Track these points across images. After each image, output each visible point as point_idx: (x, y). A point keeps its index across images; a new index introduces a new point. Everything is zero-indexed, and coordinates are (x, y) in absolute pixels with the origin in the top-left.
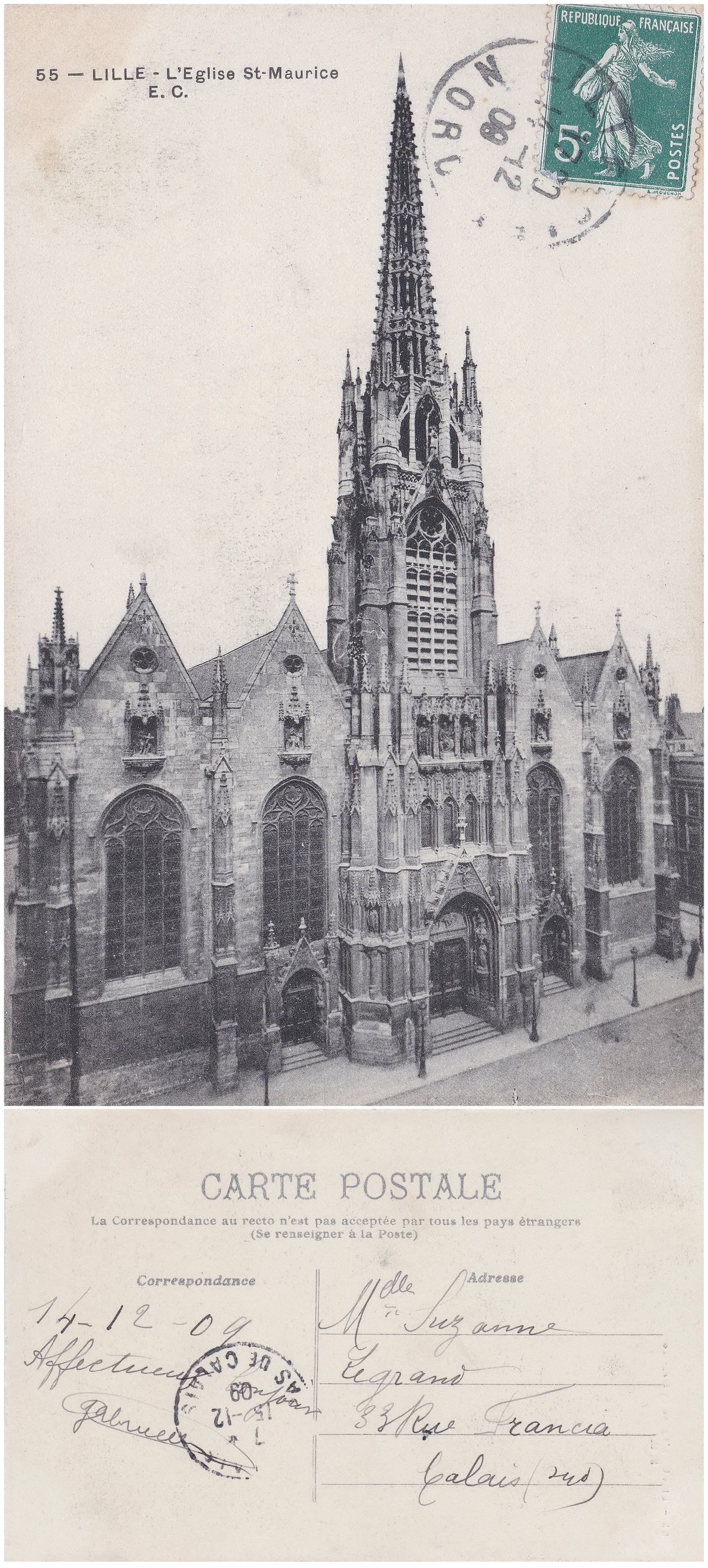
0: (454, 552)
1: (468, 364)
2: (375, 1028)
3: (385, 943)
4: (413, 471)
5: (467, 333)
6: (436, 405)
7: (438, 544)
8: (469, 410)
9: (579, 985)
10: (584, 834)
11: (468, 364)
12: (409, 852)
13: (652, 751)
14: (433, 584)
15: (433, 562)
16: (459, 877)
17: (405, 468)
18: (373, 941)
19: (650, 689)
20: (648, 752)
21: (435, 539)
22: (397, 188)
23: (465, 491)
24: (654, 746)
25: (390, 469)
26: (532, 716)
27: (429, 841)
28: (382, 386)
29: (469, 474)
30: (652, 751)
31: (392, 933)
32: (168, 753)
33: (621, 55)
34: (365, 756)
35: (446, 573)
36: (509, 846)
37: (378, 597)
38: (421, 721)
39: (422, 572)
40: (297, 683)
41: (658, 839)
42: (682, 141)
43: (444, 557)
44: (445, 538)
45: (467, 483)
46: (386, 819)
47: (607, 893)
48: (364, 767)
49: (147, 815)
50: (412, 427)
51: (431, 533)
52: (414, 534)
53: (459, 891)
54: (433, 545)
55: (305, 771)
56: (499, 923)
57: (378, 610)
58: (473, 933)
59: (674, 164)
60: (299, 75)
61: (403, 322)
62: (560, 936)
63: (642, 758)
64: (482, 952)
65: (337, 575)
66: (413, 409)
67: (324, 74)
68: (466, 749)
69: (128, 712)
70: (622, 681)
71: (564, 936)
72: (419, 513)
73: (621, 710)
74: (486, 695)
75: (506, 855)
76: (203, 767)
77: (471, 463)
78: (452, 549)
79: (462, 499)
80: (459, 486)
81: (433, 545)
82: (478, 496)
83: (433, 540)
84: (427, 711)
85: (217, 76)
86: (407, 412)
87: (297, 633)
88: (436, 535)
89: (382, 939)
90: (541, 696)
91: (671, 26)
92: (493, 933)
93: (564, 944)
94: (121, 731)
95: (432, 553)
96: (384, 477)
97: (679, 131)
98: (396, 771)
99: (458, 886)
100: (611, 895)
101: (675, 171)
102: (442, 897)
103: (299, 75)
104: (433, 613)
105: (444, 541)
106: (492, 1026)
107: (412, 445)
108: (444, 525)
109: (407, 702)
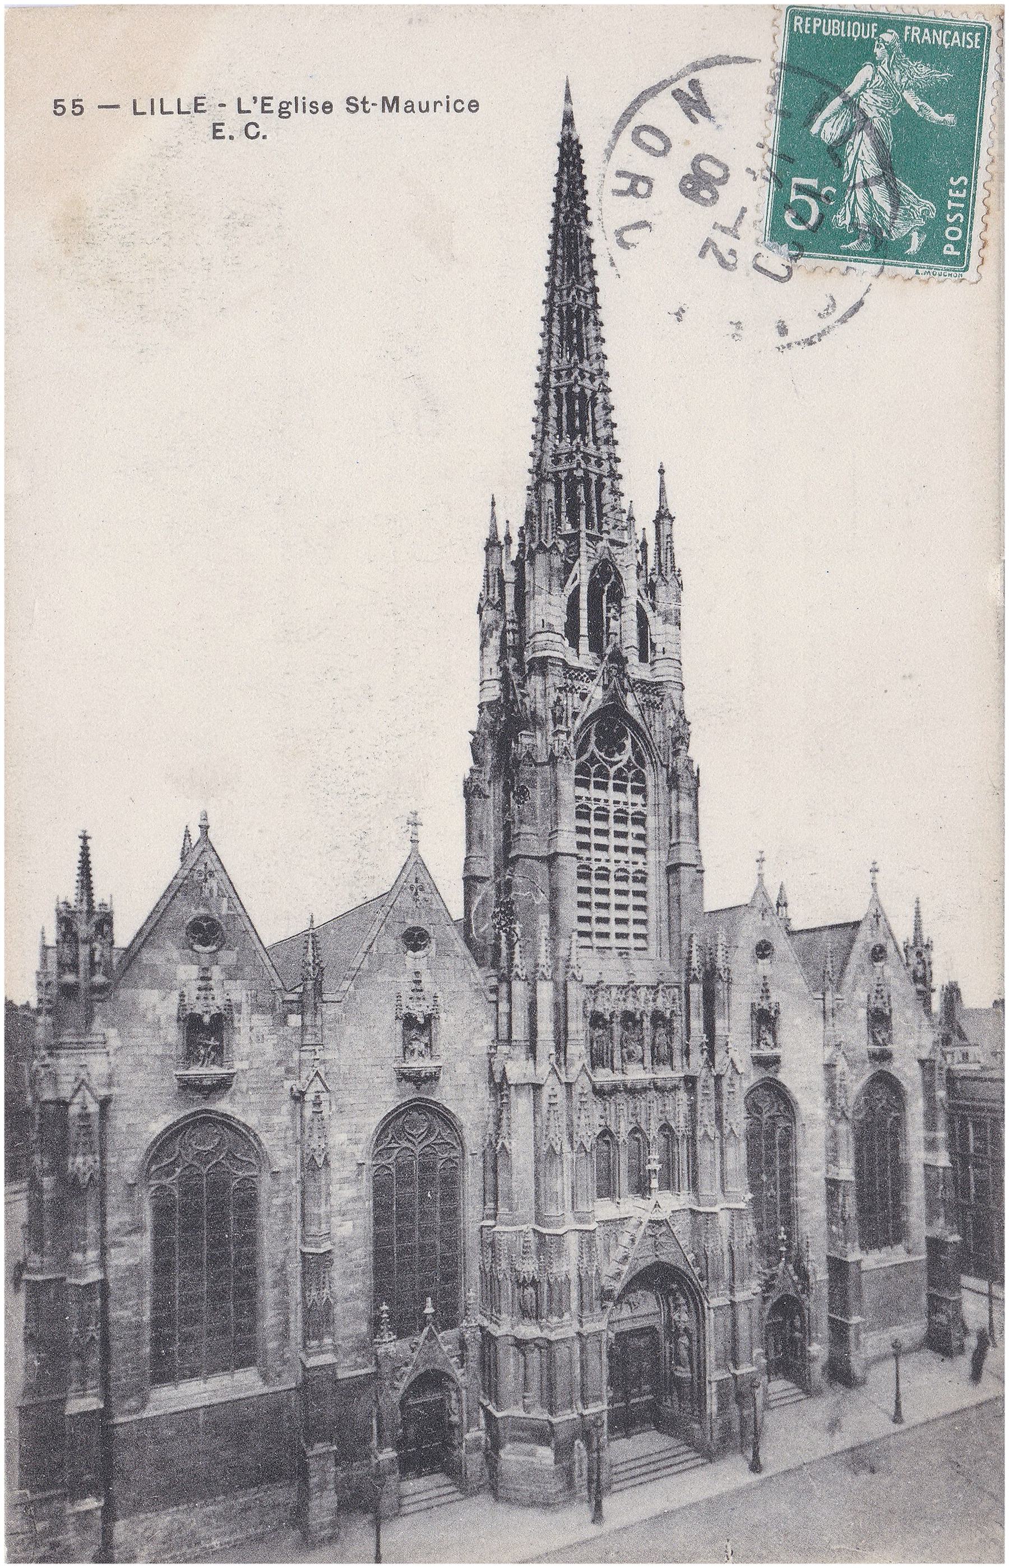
0: (643, 781)
1: (663, 516)
2: (532, 1454)
3: (545, 1334)
5: (662, 472)
6: (618, 574)
7: (620, 770)
8: (664, 580)
9: (819, 1392)
10: (826, 1179)
11: (663, 516)
14: (613, 826)
15: (613, 795)
18: (529, 1331)
19: (919, 975)
20: (916, 1064)
21: (617, 763)
22: (563, 267)
24: (924, 1055)
25: (552, 665)
26: (753, 1013)
27: (607, 1189)
28: (541, 546)
29: (664, 671)
31: (556, 1319)
32: (238, 1066)
33: (878, 79)
34: (518, 1070)
35: (631, 810)
36: (720, 1196)
37: (536, 844)
38: (596, 1020)
39: (598, 809)
40: (422, 966)
41: (931, 1186)
42: (965, 201)
43: (629, 788)
44: (629, 761)
45: (661, 683)
47: (858, 1263)
48: (516, 1086)
49: (209, 1152)
50: (584, 604)
51: (611, 754)
52: (586, 756)
53: (650, 1261)
54: (612, 771)
55: (431, 1091)
56: (706, 1305)
57: (536, 863)
58: (670, 1319)
59: (953, 234)
60: (424, 108)
62: (792, 1324)
64: (682, 1347)
66: (585, 579)
67: (459, 106)
69: (182, 1007)
70: (880, 964)
71: (798, 1324)
73: (879, 1004)
74: (688, 983)
76: (288, 1084)
78: (640, 777)
79: (653, 706)
81: (612, 771)
83: (613, 764)
84: (605, 1006)
85: (308, 108)
86: (576, 583)
87: (420, 894)
88: (617, 757)
89: (541, 1328)
90: (765, 985)
91: (949, 38)
92: (698, 1320)
94: (173, 1034)
96: (544, 675)
97: (960, 187)
98: (561, 1091)
99: (648, 1253)
100: (864, 1266)
101: (954, 243)
102: (626, 1268)
103: (424, 108)
104: (612, 867)
106: (697, 1451)
107: (584, 630)
108: (628, 743)
109: (576, 993)
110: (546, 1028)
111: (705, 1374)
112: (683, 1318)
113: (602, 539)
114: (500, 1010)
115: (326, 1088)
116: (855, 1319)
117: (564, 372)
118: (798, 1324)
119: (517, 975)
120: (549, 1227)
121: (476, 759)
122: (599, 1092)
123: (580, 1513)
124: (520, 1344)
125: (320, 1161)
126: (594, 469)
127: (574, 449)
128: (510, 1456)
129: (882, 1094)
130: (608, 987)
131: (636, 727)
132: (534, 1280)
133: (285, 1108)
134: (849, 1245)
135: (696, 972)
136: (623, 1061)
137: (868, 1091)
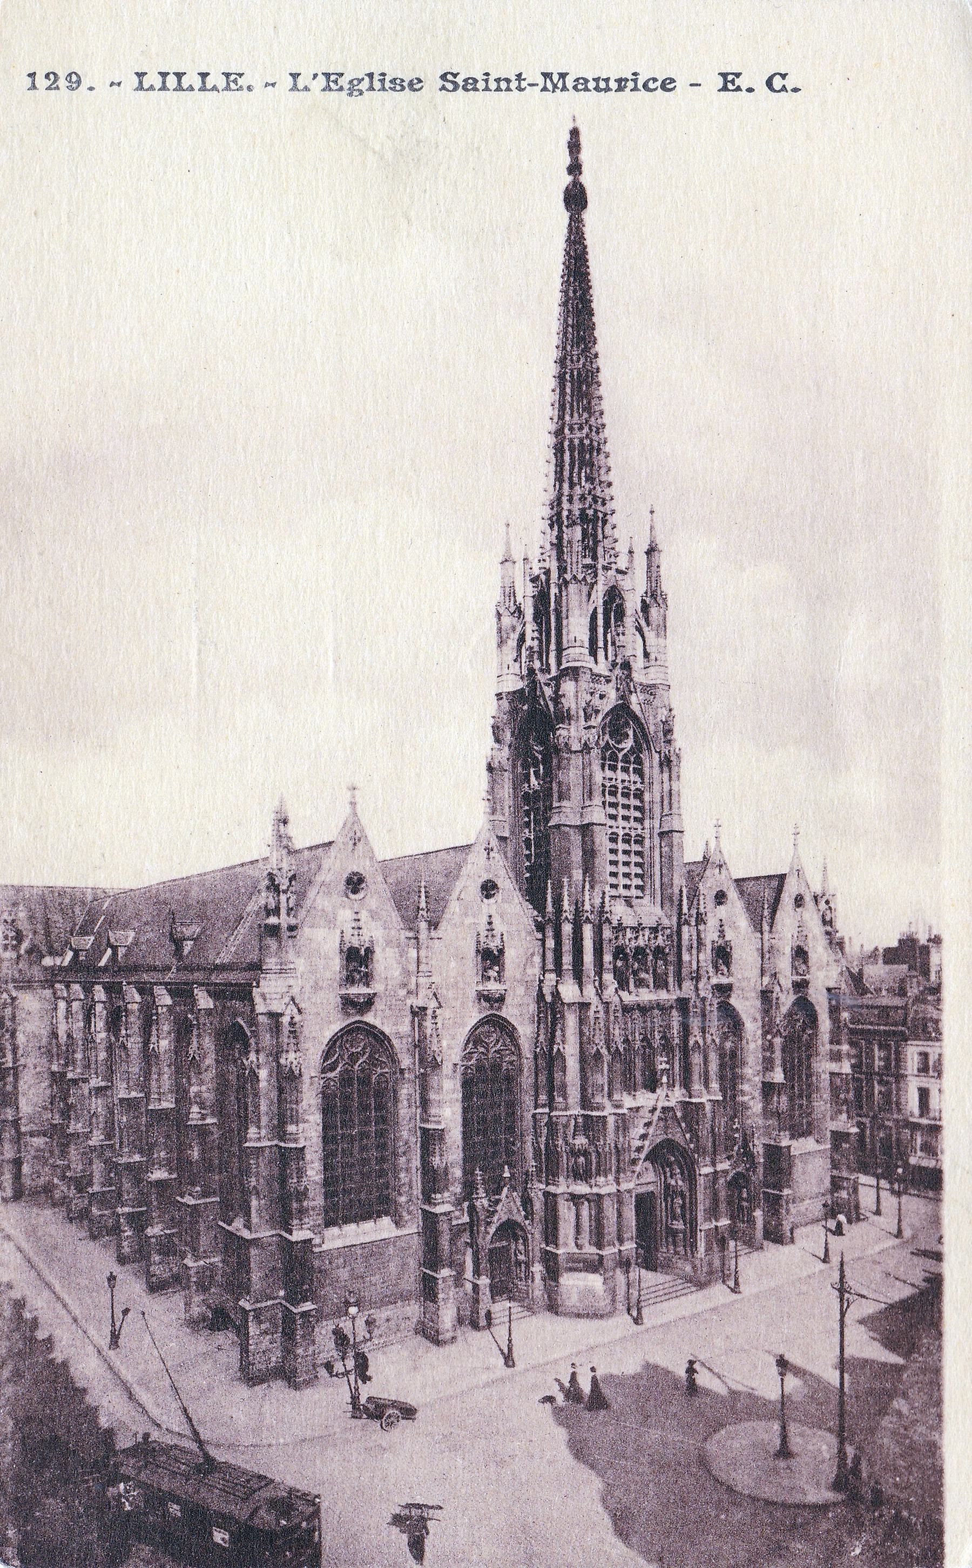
3: (595, 1190)
4: (602, 673)
6: (622, 598)
10: (762, 1082)
13: (829, 990)
14: (621, 800)
15: (621, 775)
16: (662, 1124)
17: (596, 671)
18: (581, 1188)
19: (828, 919)
21: (623, 749)
23: (651, 694)
24: (832, 984)
26: (478, 951)
28: (575, 577)
29: (653, 677)
30: (829, 990)
34: (569, 991)
36: (704, 1092)
38: (619, 952)
39: (611, 786)
41: (835, 1090)
43: (631, 769)
46: (588, 1061)
51: (619, 742)
54: (620, 756)
55: (500, 1008)
63: (819, 999)
68: (660, 983)
74: (679, 926)
75: (703, 1100)
76: (409, 1002)
77: (658, 663)
78: (639, 761)
79: (649, 703)
80: (650, 689)
81: (620, 756)
84: (630, 941)
87: (491, 853)
89: (591, 1187)
90: (721, 926)
93: (745, 1204)
94: (337, 963)
95: (620, 765)
99: (658, 1132)
104: (621, 832)
105: (632, 751)
108: (631, 733)
109: (607, 933)
110: (567, 959)
114: (547, 946)
117: (576, 426)
118: (745, 1195)
119: (566, 918)
121: (498, 740)
122: (626, 1009)
124: (575, 1199)
125: (297, 1072)
126: (600, 508)
131: (636, 718)
132: (585, 1150)
133: (408, 1020)
135: (567, 914)
137: (475, 1039)
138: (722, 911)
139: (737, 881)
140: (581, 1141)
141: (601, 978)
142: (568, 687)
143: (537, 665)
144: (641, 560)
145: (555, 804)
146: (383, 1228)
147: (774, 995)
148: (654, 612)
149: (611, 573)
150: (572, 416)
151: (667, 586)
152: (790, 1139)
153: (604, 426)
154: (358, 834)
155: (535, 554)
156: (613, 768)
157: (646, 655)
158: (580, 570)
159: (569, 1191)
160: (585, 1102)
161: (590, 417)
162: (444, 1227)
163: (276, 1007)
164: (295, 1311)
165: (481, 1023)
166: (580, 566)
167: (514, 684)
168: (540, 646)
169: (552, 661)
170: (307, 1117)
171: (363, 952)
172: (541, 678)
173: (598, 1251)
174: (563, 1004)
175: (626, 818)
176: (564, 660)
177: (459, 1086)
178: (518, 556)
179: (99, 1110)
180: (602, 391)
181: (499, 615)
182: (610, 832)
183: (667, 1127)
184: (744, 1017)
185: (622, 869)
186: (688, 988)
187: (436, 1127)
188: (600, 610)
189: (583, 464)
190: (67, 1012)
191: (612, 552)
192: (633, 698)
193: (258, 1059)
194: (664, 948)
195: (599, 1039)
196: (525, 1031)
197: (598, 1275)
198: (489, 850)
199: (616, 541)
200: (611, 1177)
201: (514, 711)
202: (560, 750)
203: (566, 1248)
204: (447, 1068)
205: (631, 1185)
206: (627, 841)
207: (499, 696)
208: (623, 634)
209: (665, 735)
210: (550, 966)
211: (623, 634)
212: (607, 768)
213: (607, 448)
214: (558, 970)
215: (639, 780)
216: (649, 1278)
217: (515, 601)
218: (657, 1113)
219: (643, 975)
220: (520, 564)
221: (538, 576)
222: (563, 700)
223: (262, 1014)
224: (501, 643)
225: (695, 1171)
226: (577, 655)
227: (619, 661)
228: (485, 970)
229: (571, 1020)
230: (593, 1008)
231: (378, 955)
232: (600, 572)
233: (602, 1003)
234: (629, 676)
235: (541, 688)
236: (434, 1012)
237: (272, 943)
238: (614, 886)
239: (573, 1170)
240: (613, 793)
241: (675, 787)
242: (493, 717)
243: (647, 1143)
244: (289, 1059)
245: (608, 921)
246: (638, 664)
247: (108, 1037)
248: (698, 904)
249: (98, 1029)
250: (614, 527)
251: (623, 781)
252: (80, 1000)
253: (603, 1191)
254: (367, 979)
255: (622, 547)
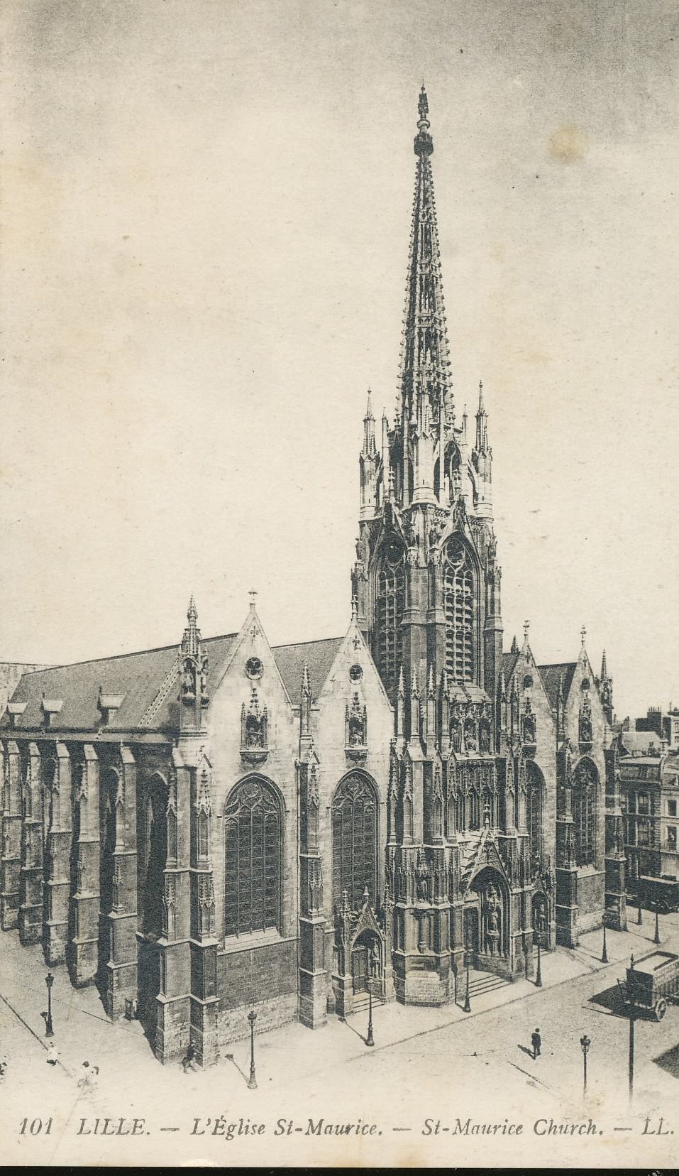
0: (471, 578)
6: (458, 451)
7: (459, 571)
9: (555, 950)
12: (450, 835)
15: (456, 587)
16: (485, 855)
18: (425, 905)
19: (606, 698)
21: (458, 566)
24: (608, 747)
29: (482, 511)
32: (270, 747)
34: (415, 752)
38: (454, 723)
43: (455, 580)
45: (481, 518)
47: (575, 872)
51: (455, 561)
54: (456, 571)
61: (429, 373)
64: (494, 918)
65: (360, 589)
68: (484, 747)
70: (587, 691)
71: (543, 910)
72: (447, 544)
80: (479, 520)
81: (456, 571)
82: (491, 530)
83: (456, 567)
88: (458, 564)
99: (483, 861)
105: (464, 568)
106: (502, 977)
111: (509, 933)
112: (496, 901)
113: (450, 428)
115: (318, 761)
116: (574, 906)
118: (543, 910)
120: (433, 845)
121: (359, 557)
123: (454, 1011)
124: (418, 914)
126: (442, 382)
127: (432, 369)
128: (412, 978)
129: (358, 791)
130: (459, 704)
134: (571, 862)
136: (466, 749)
138: (528, 693)
139: (540, 667)
140: (424, 868)
141: (440, 743)
142: (418, 518)
143: (393, 500)
144: (472, 422)
145: (407, 608)
146: (270, 936)
147: (567, 755)
148: (481, 462)
149: (451, 431)
150: (420, 310)
151: (491, 442)
152: (577, 866)
153: (445, 319)
154: (257, 629)
155: (391, 416)
156: (450, 581)
157: (475, 495)
158: (427, 429)
159: (414, 906)
160: (428, 837)
161: (435, 312)
162: (316, 934)
163: (192, 762)
164: (203, 1003)
165: (347, 777)
166: (428, 425)
167: (370, 515)
168: (395, 486)
169: (406, 499)
170: (213, 849)
171: (259, 720)
172: (396, 510)
173: (436, 955)
174: (411, 762)
175: (459, 619)
176: (414, 497)
177: (330, 824)
178: (377, 416)
179: (32, 842)
180: (445, 292)
181: (362, 461)
182: (447, 630)
183: (488, 857)
184: (544, 772)
185: (457, 659)
186: (504, 752)
187: (315, 856)
188: (442, 461)
189: (428, 346)
190: (5, 763)
191: (451, 416)
192: (466, 529)
193: (176, 803)
194: (487, 720)
195: (439, 789)
196: (382, 780)
197: (435, 973)
198: (356, 642)
199: (453, 407)
200: (446, 897)
201: (374, 536)
202: (411, 566)
203: (411, 951)
204: (322, 812)
205: (462, 903)
206: (460, 636)
207: (362, 524)
208: (459, 479)
209: (489, 557)
210: (400, 732)
211: (459, 479)
212: (445, 581)
213: (447, 336)
214: (407, 735)
215: (469, 590)
216: (476, 975)
217: (375, 451)
218: (481, 847)
219: (471, 740)
220: (379, 423)
221: (394, 432)
222: (413, 528)
223: (181, 768)
224: (363, 483)
225: (508, 892)
226: (424, 494)
227: (456, 498)
228: (352, 734)
229: (418, 774)
230: (434, 765)
231: (271, 721)
232: (442, 430)
233: (442, 761)
234: (463, 511)
235: (396, 518)
236: (313, 767)
237: (188, 713)
238: (450, 672)
239: (418, 891)
240: (450, 600)
241: (496, 597)
242: (357, 539)
243: (473, 870)
244: (201, 802)
245: (447, 698)
246: (469, 502)
247: (40, 784)
248: (513, 686)
249: (32, 778)
250: (452, 396)
251: (458, 591)
252: (16, 753)
253: (440, 907)
254: (262, 741)
255: (458, 412)
